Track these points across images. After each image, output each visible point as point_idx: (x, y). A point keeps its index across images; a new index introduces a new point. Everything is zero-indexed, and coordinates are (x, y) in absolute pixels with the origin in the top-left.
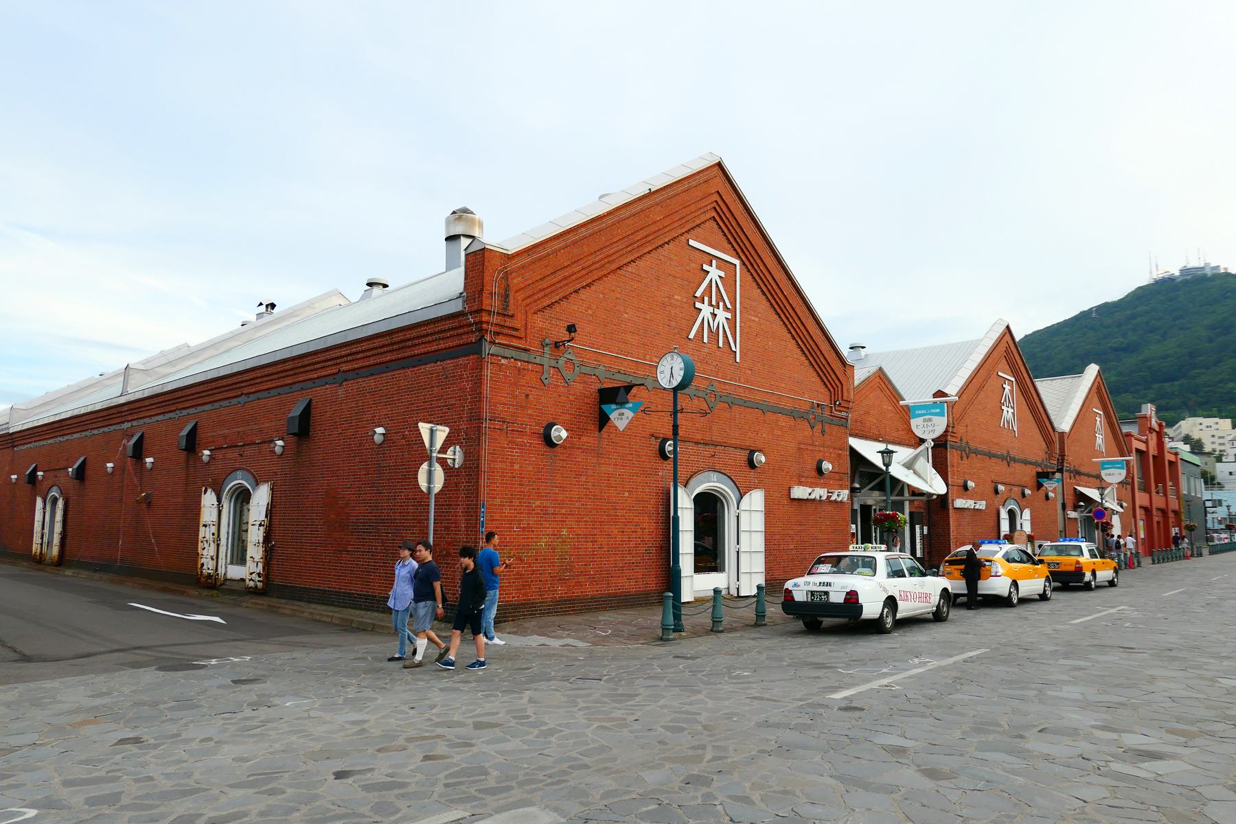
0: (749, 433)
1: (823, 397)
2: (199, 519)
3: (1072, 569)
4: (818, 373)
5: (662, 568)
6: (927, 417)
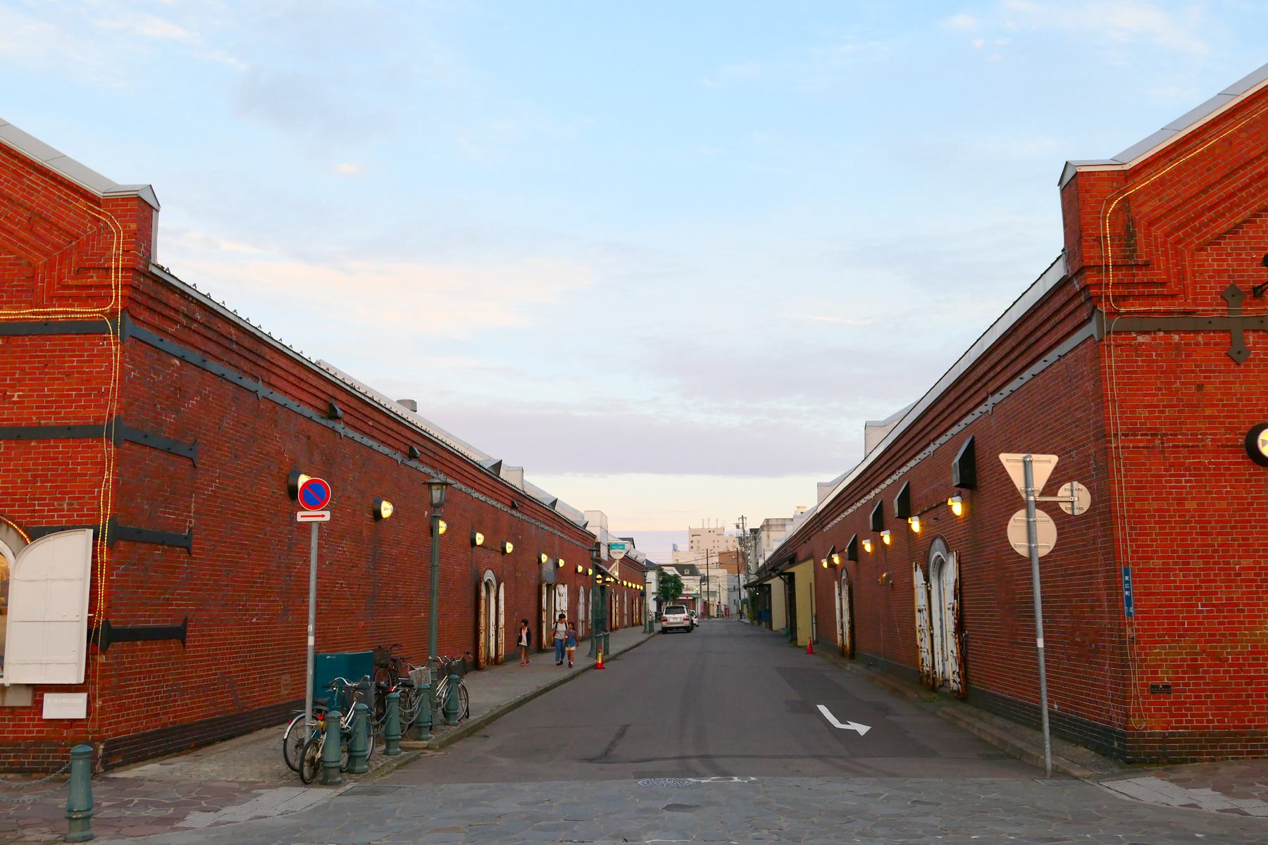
2: (914, 603)
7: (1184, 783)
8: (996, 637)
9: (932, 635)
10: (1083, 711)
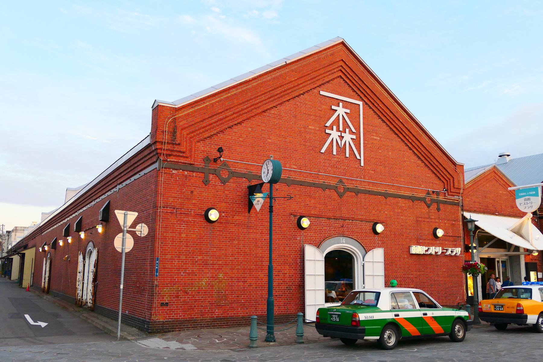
0: (374, 211)
1: (438, 186)
2: (77, 269)
3: (514, 311)
4: (432, 171)
5: (301, 299)
6: (527, 197)
7: (167, 340)
8: (109, 284)
9: (83, 283)
10: (136, 313)
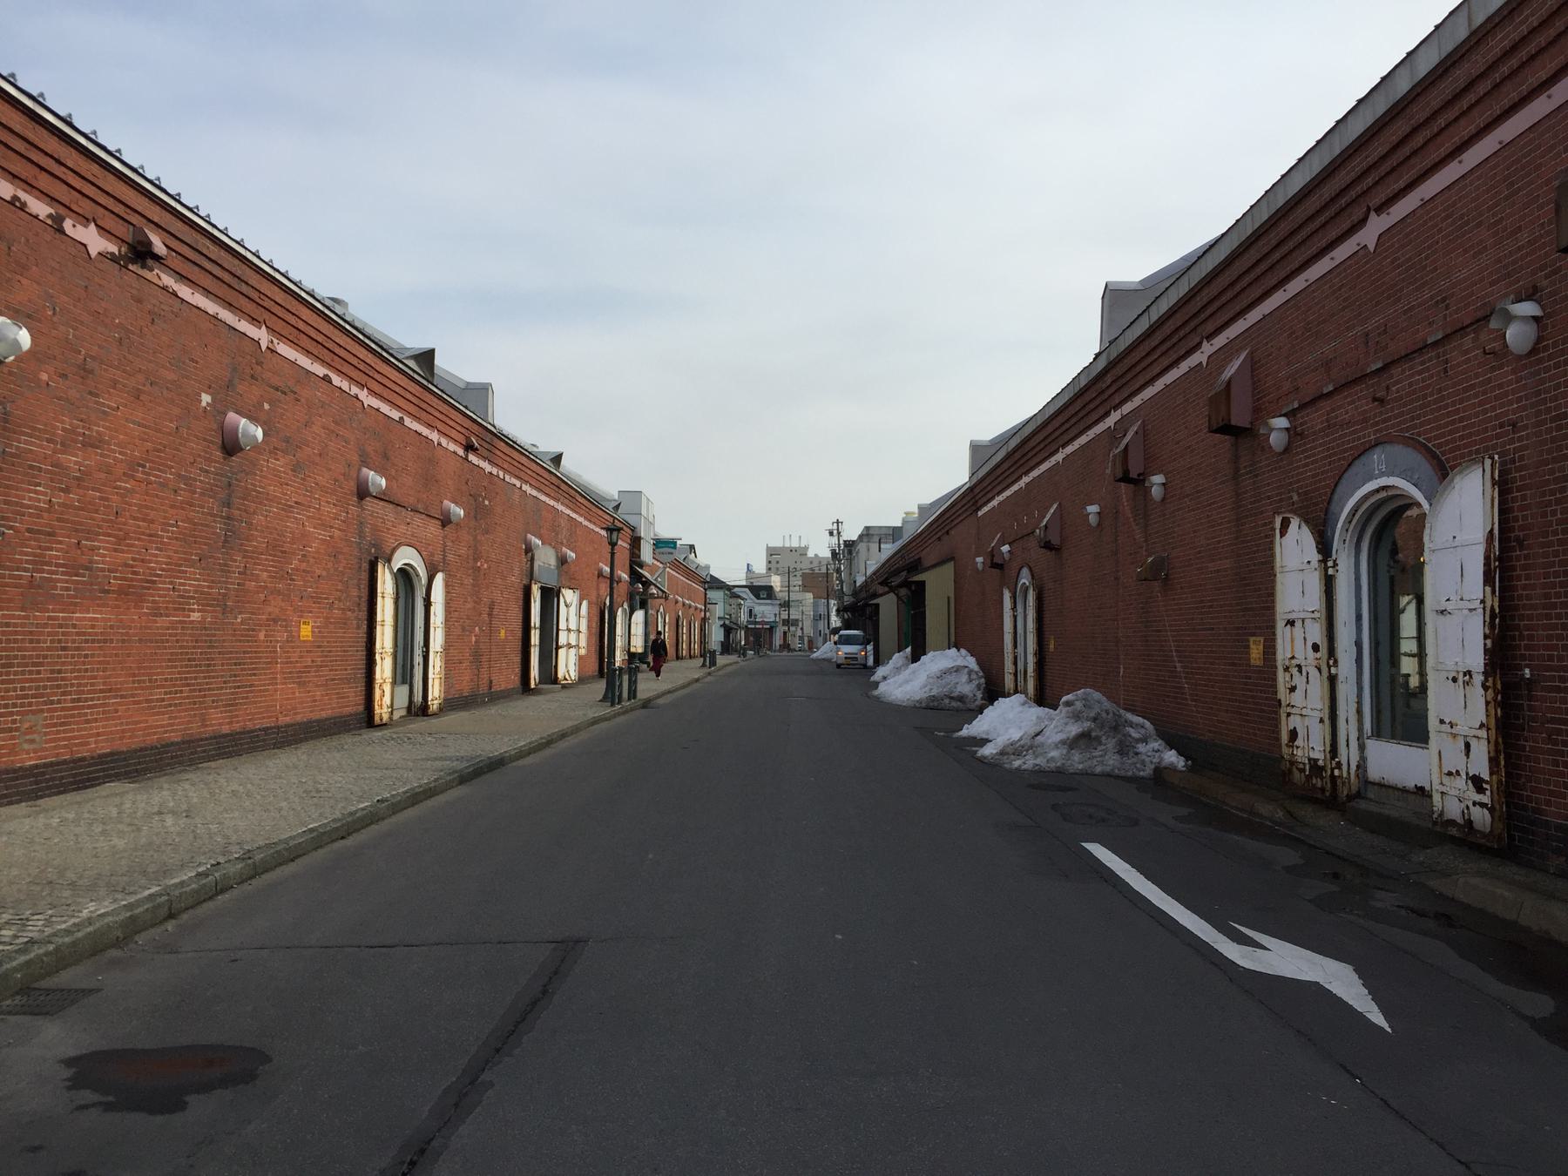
9: (1332, 680)
